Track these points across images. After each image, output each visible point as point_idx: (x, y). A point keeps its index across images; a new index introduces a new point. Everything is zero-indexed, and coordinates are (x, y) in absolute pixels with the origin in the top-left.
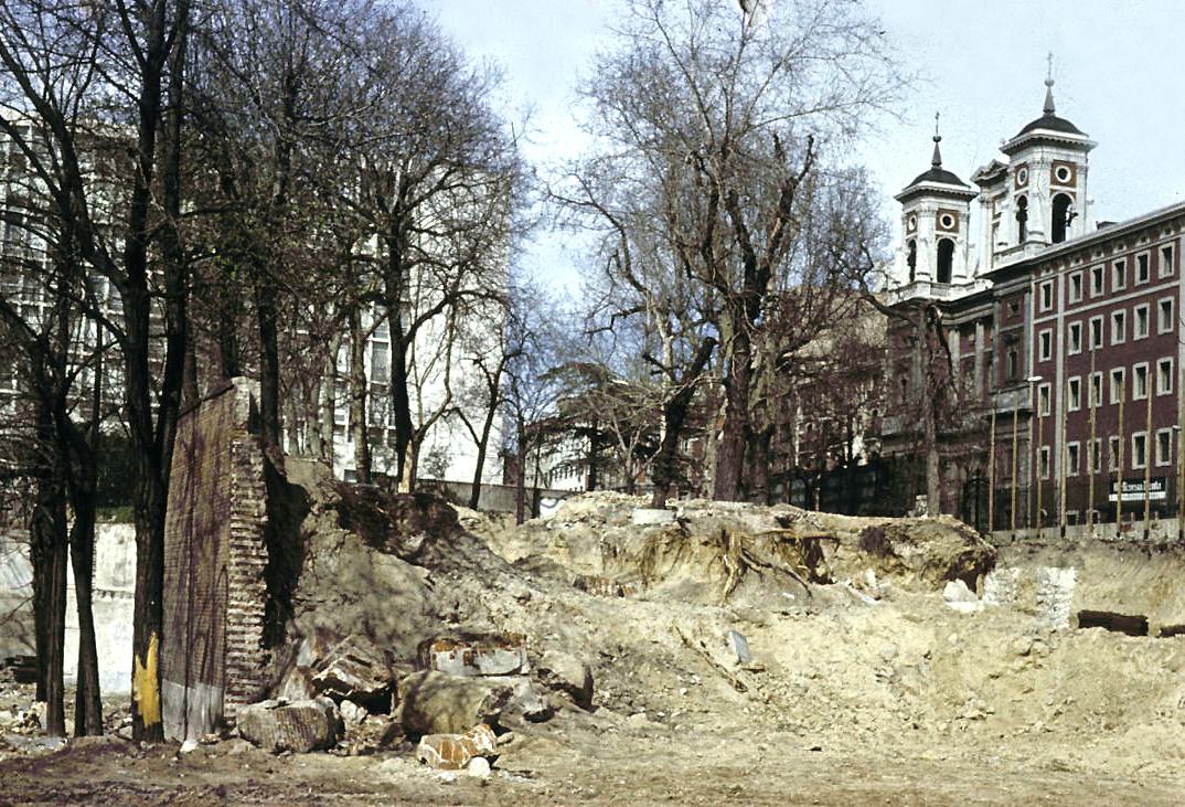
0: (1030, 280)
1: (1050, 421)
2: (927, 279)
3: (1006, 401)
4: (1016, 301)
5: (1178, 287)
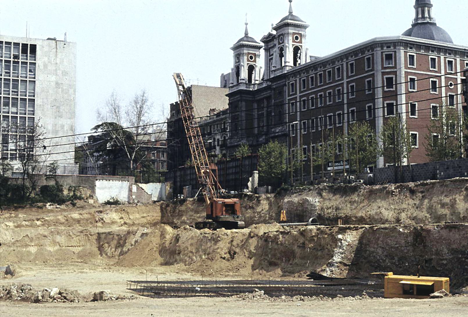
0: (286, 81)
1: (295, 138)
2: (244, 82)
3: (277, 131)
4: (280, 92)
5: (374, 74)
